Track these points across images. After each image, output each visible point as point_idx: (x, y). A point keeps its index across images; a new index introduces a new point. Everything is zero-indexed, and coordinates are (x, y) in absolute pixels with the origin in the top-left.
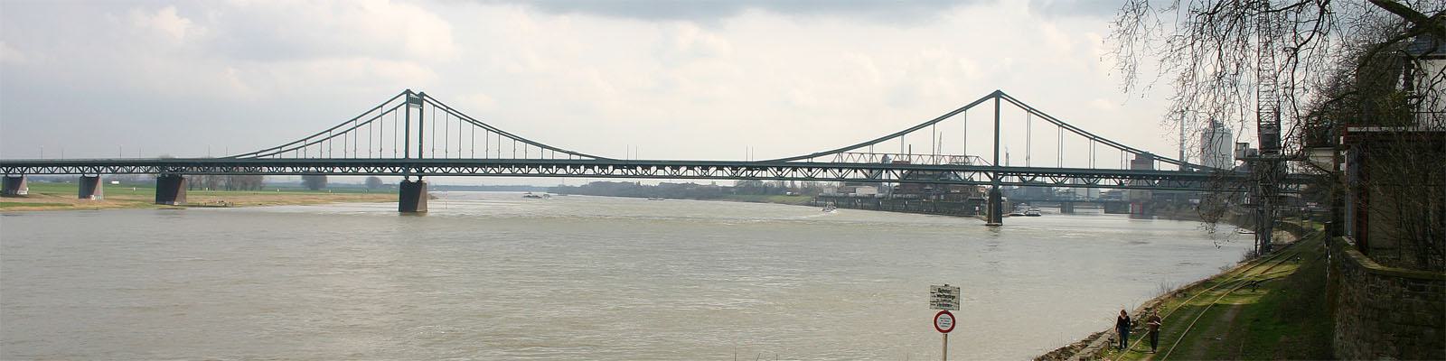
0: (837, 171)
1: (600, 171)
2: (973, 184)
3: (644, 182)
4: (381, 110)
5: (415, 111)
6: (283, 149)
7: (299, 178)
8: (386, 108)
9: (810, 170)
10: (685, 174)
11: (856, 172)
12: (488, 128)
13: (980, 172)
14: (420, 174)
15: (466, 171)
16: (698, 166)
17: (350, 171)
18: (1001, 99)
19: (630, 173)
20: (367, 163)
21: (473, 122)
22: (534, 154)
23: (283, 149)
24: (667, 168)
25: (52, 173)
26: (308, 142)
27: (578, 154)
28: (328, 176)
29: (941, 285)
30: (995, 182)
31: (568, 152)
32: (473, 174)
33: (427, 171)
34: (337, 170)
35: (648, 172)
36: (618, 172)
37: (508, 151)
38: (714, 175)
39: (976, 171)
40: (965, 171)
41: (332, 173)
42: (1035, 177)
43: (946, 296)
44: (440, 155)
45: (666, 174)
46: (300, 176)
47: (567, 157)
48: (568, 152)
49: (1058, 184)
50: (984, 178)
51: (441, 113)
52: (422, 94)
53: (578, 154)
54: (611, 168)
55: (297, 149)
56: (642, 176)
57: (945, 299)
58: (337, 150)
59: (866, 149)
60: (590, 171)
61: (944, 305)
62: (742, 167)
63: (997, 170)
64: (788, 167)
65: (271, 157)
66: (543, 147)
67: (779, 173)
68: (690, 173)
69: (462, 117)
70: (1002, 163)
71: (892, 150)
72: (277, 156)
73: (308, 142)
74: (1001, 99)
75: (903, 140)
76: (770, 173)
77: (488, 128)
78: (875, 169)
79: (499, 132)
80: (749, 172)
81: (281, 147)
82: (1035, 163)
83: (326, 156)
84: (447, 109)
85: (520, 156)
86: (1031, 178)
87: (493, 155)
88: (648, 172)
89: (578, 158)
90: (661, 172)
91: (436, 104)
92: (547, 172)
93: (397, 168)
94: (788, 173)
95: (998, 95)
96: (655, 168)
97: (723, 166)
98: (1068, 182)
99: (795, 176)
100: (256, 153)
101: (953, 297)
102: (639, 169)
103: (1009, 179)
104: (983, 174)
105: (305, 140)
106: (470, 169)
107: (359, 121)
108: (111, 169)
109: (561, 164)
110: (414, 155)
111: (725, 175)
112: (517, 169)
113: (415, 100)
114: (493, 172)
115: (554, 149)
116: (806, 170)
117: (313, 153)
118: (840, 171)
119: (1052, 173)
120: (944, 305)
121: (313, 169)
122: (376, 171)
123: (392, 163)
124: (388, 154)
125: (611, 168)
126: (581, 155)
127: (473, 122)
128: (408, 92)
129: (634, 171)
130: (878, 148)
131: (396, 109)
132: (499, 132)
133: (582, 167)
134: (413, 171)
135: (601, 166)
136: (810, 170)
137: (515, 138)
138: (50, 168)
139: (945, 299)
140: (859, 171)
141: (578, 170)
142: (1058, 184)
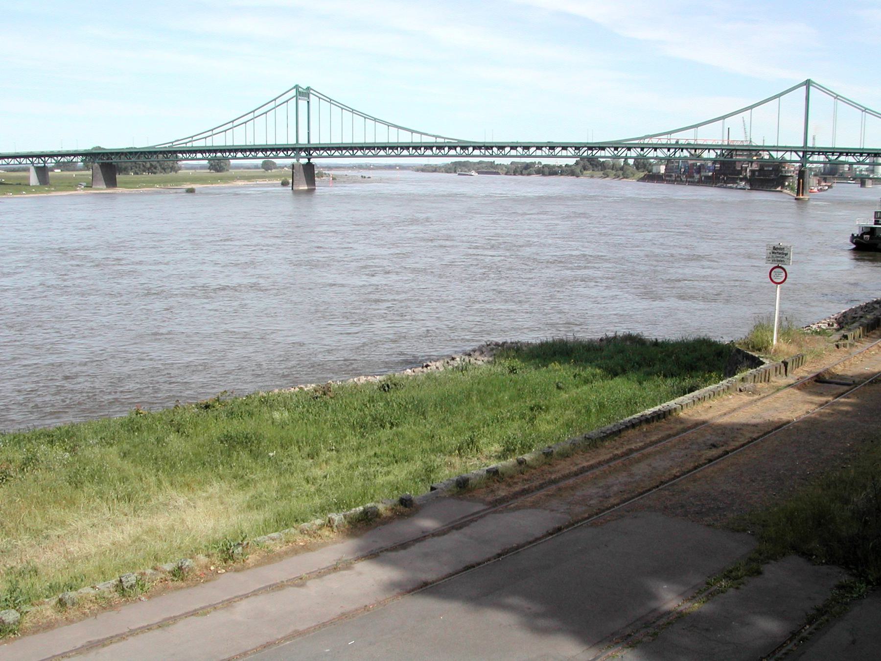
0: (666, 150)
1: (462, 151)
2: (783, 162)
3: (498, 161)
4: (275, 103)
5: (303, 104)
6: (194, 138)
7: (206, 162)
8: (279, 101)
9: (642, 149)
10: (534, 154)
11: (682, 151)
12: (366, 117)
13: (791, 151)
14: (309, 157)
15: (347, 154)
16: (571, 147)
17: (251, 156)
18: (805, 87)
19: (487, 153)
20: (264, 150)
21: (353, 111)
22: (405, 138)
23: (194, 138)
24: (519, 149)
25: (8, 164)
26: (215, 131)
27: (443, 138)
28: (231, 160)
29: (776, 244)
30: (804, 158)
31: (433, 136)
32: (353, 156)
33: (314, 154)
34: (239, 155)
35: (503, 152)
36: (477, 152)
37: (383, 136)
38: (560, 154)
39: (787, 151)
40: (777, 151)
41: (235, 158)
42: (839, 156)
43: (780, 253)
44: (325, 140)
45: (519, 154)
46: (207, 161)
47: (433, 140)
48: (433, 136)
49: (859, 163)
50: (795, 157)
51: (325, 105)
52: (308, 88)
53: (443, 138)
54: (471, 149)
55: (205, 138)
56: (497, 156)
57: (779, 255)
58: (238, 138)
59: (665, 137)
60: (452, 152)
61: (778, 261)
62: (583, 147)
63: (806, 152)
64: (623, 148)
65: (184, 145)
66: (412, 131)
67: (616, 152)
68: (539, 152)
69: (343, 107)
70: (810, 144)
71: (684, 138)
72: (189, 145)
73: (215, 131)
74: (811, 87)
75: (723, 123)
76: (608, 153)
77: (366, 117)
78: (699, 149)
79: (375, 120)
80: (590, 152)
81: (192, 137)
82: (840, 144)
83: (229, 143)
84: (331, 101)
85: (382, 139)
86: (836, 157)
87: (370, 140)
88: (503, 152)
89: (442, 140)
90: (513, 152)
91: (321, 97)
92: (416, 154)
93: (289, 152)
94: (623, 152)
95: (808, 83)
96: (535, 149)
97: (542, 147)
98: (868, 161)
99: (628, 155)
100: (172, 143)
101: (786, 254)
102: (495, 149)
103: (815, 158)
104: (793, 153)
105: (212, 130)
106: (351, 152)
107: (257, 113)
108: (54, 160)
109: (429, 147)
110: (303, 141)
111: (569, 154)
112: (391, 151)
113: (303, 93)
114: (370, 154)
115: (422, 134)
116: (639, 150)
117: (219, 141)
118: (669, 151)
119: (855, 153)
120: (778, 261)
121: (219, 154)
122: (272, 155)
123: (285, 149)
124: (282, 141)
125: (471, 149)
126: (445, 138)
127: (353, 111)
128: (297, 87)
129: (490, 151)
130: (674, 136)
131: (287, 101)
132: (375, 120)
133: (446, 149)
134: (303, 154)
135: (463, 148)
136: (642, 149)
137: (389, 125)
138: (18, 159)
139: (779, 255)
140: (684, 151)
141: (442, 151)
142: (859, 163)
